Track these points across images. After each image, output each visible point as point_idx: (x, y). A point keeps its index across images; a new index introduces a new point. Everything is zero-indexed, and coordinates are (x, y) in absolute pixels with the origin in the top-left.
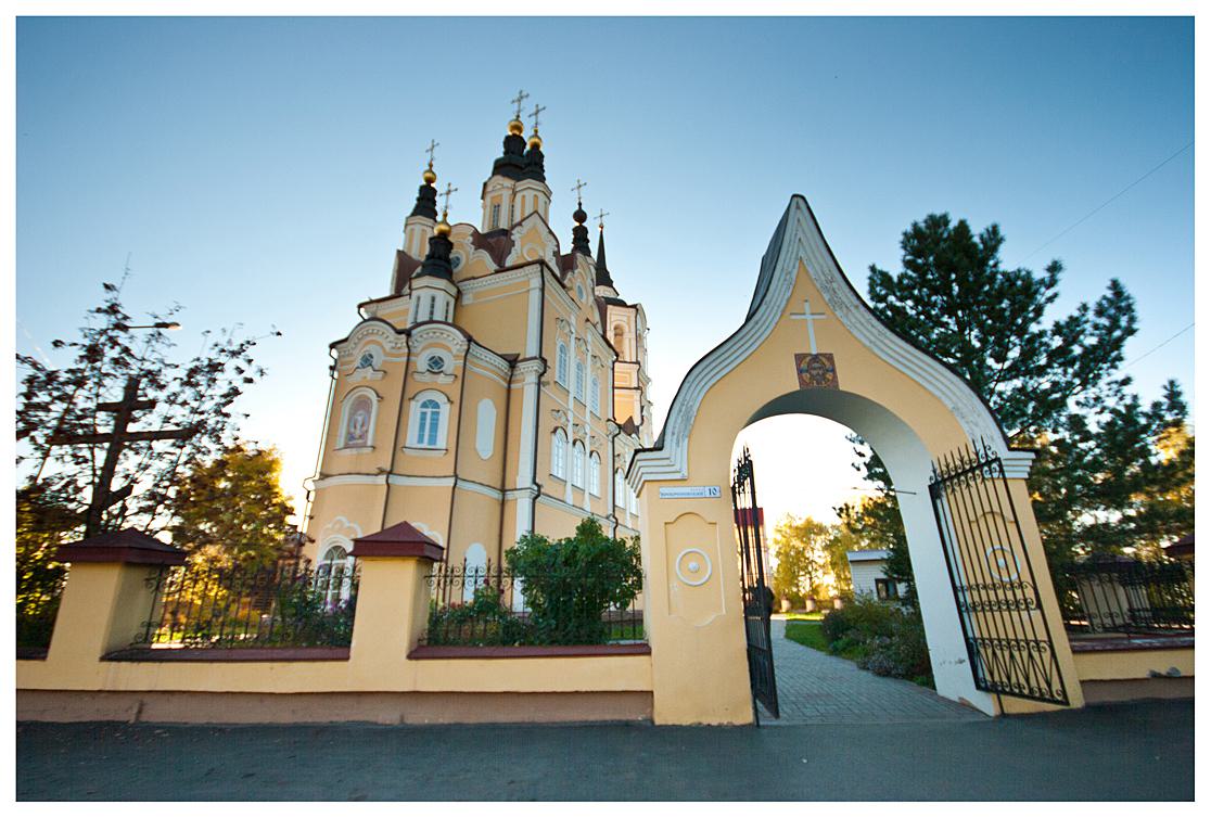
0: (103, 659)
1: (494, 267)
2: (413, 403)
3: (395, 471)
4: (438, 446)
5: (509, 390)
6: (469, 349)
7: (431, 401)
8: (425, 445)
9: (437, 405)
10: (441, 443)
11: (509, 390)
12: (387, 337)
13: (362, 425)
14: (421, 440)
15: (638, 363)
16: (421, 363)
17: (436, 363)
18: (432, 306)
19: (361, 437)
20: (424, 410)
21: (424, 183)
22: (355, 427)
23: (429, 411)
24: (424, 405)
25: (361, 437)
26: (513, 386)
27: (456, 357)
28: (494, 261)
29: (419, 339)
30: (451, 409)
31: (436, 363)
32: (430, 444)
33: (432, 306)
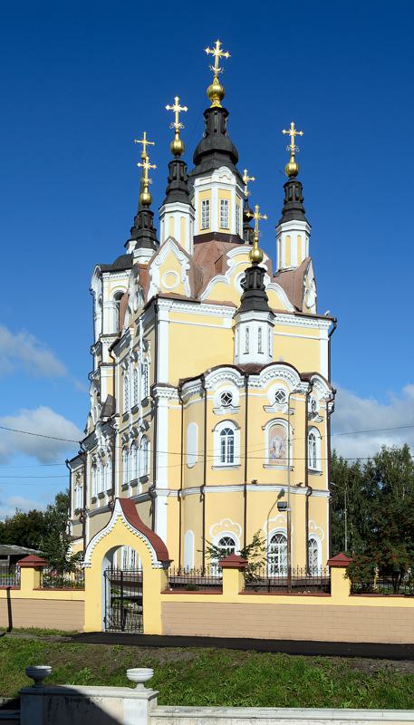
1: (187, 292)
7: (227, 429)
8: (226, 464)
9: (231, 432)
10: (237, 461)
17: (227, 398)
23: (226, 436)
24: (223, 433)
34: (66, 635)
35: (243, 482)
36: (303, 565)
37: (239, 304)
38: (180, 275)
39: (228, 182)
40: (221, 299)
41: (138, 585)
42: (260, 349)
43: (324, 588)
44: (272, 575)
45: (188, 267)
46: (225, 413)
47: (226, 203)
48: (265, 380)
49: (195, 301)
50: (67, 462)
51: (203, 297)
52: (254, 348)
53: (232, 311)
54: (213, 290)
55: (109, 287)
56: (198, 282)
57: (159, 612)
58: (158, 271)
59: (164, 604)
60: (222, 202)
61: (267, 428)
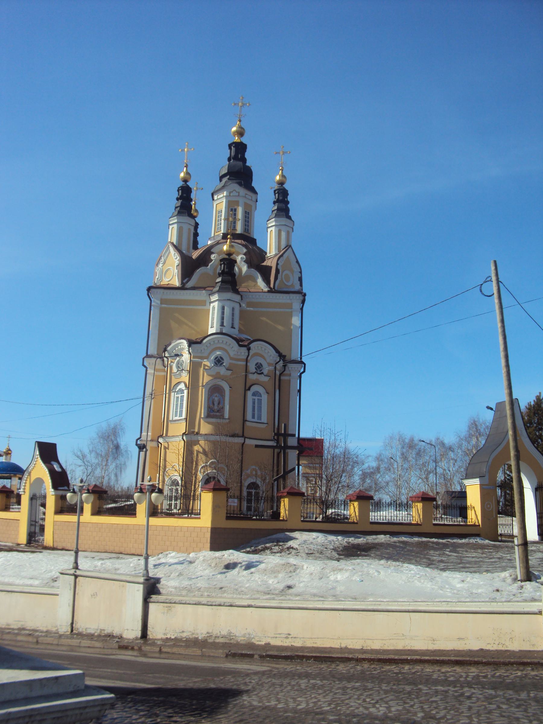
4: (262, 421)
6: (279, 362)
8: (256, 420)
12: (230, 344)
13: (219, 404)
14: (253, 417)
15: (300, 292)
16: (252, 367)
19: (218, 411)
20: (254, 397)
22: (214, 404)
23: (256, 398)
25: (218, 411)
27: (269, 364)
31: (259, 366)
42: (233, 324)
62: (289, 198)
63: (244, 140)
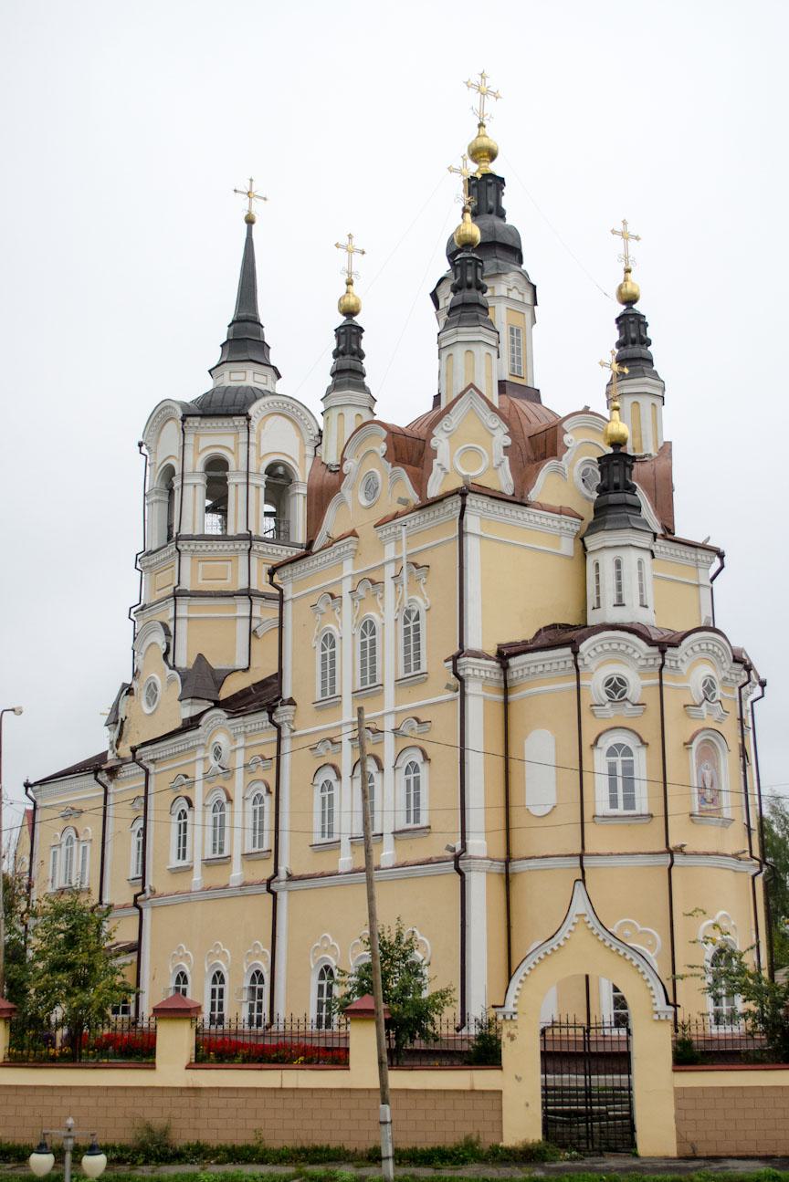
0: (187, 1068)
2: (597, 753)
3: (578, 858)
5: (506, 703)
7: (619, 746)
8: (620, 811)
9: (628, 752)
10: (642, 806)
11: (506, 703)
17: (616, 687)
18: (619, 577)
20: (612, 759)
21: (341, 319)
23: (619, 760)
24: (611, 752)
26: (511, 697)
28: (415, 490)
29: (685, 658)
30: (648, 755)
32: (625, 808)
33: (619, 577)
34: (661, 1157)
35: (579, 851)
36: (566, 1021)
37: (590, 516)
38: (490, 453)
39: (519, 298)
40: (556, 503)
41: (621, 1060)
42: (620, 597)
43: (337, 1057)
44: (714, 1031)
45: (508, 441)
46: (611, 713)
47: (518, 331)
48: (685, 658)
49: (519, 500)
50: (27, 786)
51: (533, 495)
52: (609, 596)
53: (573, 526)
54: (546, 486)
55: (196, 446)
56: (524, 478)
57: (670, 1110)
58: (446, 442)
59: (681, 1094)
60: (512, 329)
61: (694, 745)
62: (651, 333)
63: (496, 168)
